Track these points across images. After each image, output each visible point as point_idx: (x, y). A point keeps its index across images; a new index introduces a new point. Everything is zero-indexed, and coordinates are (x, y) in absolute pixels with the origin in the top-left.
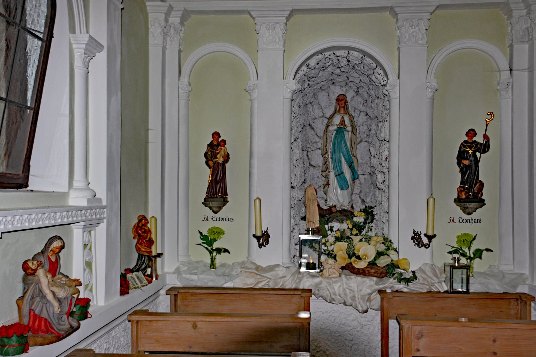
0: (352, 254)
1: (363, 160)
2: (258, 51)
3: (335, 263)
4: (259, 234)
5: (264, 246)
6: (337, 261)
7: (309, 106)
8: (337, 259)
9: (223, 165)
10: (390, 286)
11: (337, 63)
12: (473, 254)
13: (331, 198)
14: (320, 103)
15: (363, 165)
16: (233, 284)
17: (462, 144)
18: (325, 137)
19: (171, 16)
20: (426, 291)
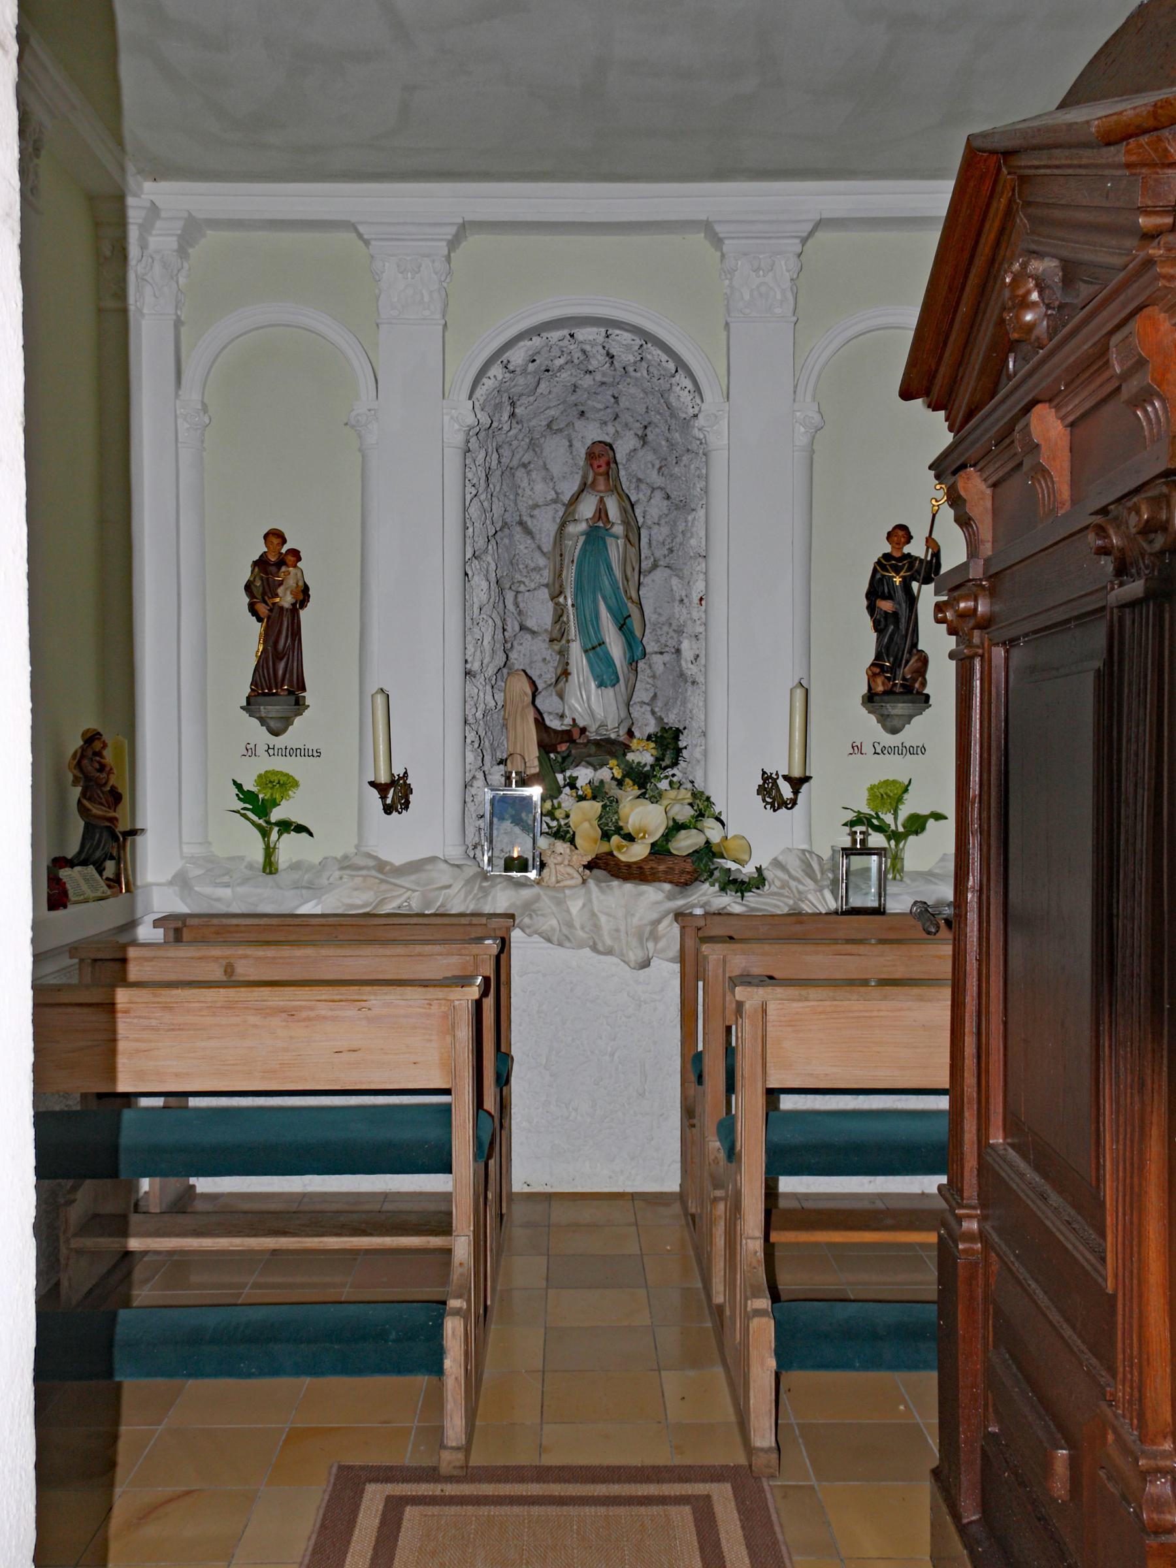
0: (611, 828)
1: (660, 614)
2: (377, 325)
3: (571, 850)
4: (383, 779)
5: (397, 811)
6: (576, 848)
7: (520, 473)
8: (578, 841)
9: (294, 611)
10: (701, 903)
11: (581, 358)
12: (904, 827)
13: (571, 708)
14: (548, 467)
15: (661, 628)
16: (320, 906)
17: (879, 563)
18: (558, 552)
19: (154, 232)
20: (786, 910)
